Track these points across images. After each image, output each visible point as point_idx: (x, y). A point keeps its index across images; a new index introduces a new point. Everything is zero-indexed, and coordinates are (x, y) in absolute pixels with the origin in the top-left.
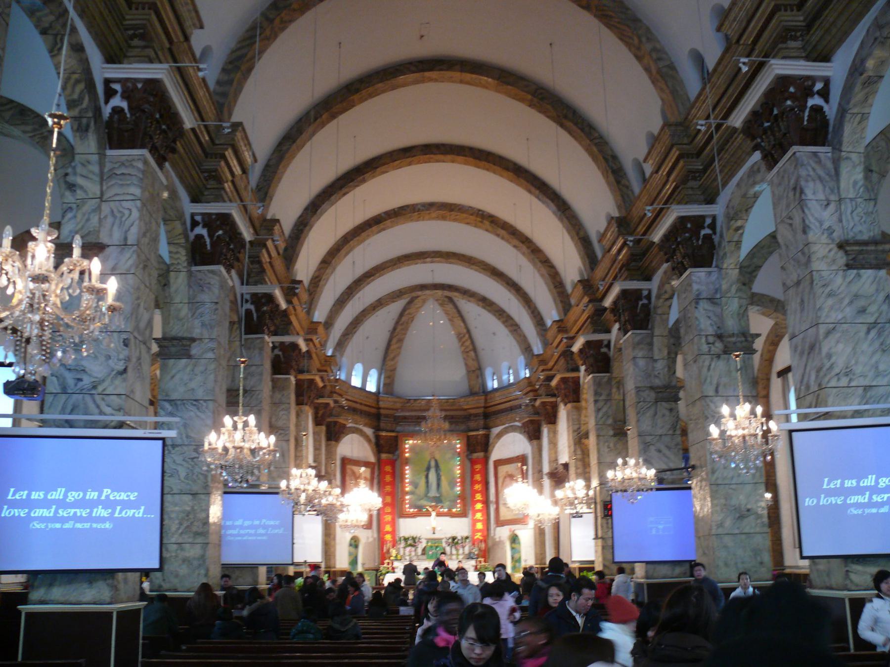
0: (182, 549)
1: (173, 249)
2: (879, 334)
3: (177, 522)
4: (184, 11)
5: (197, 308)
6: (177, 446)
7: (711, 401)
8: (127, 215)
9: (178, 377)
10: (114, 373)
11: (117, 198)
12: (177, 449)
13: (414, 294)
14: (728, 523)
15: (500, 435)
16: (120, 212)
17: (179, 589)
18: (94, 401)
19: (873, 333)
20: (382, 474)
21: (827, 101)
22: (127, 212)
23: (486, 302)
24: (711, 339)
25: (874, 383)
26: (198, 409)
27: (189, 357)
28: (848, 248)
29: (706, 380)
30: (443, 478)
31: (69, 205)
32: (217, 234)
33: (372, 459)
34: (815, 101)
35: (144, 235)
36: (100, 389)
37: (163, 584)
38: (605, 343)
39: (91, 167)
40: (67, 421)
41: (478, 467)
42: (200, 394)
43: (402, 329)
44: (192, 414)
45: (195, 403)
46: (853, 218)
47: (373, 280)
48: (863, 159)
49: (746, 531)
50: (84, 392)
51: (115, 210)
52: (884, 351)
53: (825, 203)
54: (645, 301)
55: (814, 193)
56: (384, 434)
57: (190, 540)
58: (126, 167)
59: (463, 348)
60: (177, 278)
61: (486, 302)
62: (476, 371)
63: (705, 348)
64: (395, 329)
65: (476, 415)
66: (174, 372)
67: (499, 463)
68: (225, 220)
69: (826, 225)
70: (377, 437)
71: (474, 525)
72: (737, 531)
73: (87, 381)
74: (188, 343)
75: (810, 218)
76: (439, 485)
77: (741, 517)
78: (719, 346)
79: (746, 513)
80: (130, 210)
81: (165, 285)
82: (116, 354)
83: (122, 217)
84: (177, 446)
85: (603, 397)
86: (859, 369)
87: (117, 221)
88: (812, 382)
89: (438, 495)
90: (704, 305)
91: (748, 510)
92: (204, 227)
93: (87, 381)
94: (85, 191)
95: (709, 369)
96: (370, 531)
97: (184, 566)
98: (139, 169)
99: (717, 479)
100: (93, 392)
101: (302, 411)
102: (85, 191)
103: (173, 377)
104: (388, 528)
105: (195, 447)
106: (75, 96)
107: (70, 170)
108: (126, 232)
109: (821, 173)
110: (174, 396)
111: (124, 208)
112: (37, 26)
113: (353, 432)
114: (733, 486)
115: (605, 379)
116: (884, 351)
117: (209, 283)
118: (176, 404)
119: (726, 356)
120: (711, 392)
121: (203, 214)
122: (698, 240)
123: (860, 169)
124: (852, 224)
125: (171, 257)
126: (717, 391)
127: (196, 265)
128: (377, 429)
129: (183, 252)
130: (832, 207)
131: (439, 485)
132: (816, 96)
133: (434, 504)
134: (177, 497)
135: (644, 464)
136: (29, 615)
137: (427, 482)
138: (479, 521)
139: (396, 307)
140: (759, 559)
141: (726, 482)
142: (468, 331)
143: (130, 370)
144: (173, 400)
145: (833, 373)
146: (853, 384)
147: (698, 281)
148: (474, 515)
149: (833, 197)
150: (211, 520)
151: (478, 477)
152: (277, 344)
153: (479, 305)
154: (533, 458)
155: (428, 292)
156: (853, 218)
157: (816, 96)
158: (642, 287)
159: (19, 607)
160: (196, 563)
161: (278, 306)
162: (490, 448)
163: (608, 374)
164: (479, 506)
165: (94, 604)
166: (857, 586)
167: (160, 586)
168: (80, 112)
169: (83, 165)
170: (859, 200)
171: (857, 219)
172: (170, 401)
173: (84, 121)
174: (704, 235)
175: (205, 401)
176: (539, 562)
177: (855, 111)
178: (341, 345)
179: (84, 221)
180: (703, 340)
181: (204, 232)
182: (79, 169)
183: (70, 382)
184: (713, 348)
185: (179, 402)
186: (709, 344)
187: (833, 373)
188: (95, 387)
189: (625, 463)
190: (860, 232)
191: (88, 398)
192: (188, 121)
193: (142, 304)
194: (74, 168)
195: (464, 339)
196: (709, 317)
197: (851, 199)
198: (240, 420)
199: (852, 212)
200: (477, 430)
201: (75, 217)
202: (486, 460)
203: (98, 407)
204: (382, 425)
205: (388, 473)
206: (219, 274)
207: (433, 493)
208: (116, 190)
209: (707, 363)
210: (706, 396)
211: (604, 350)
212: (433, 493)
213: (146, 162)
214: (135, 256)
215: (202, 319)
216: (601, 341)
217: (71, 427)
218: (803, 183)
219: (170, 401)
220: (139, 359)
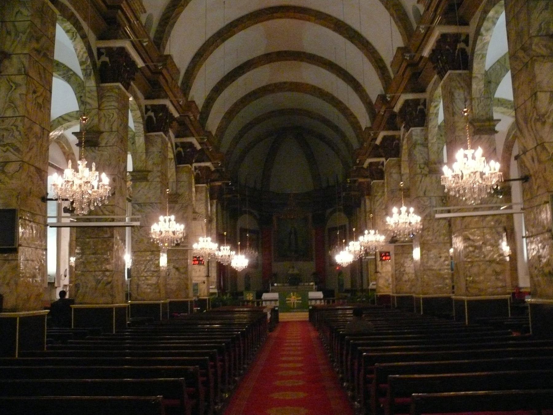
1: (136, 125)
3: (143, 266)
4: (136, 6)
7: (422, 199)
8: (112, 117)
15: (331, 213)
16: (108, 115)
21: (467, 45)
22: (112, 115)
24: (422, 166)
26: (152, 208)
27: (148, 181)
28: (475, 124)
29: (419, 188)
34: (461, 45)
35: (121, 125)
39: (93, 93)
40: (87, 219)
42: (153, 200)
44: (149, 210)
45: (150, 204)
48: (484, 77)
51: (106, 114)
54: (397, 141)
60: (139, 139)
63: (419, 171)
68: (164, 108)
75: (456, 108)
78: (427, 169)
80: (113, 114)
81: (133, 143)
90: (419, 148)
92: (152, 111)
95: (421, 182)
98: (116, 93)
106: (84, 60)
108: (112, 125)
110: (140, 201)
112: (64, 29)
115: (381, 184)
118: (141, 206)
120: (421, 194)
121: (106, 48)
122: (416, 112)
124: (478, 111)
125: (135, 129)
126: (425, 194)
129: (142, 126)
130: (468, 103)
132: (462, 43)
134: (143, 253)
135: (378, 234)
136: (75, 309)
143: (116, 193)
144: (140, 203)
147: (416, 134)
149: (468, 97)
150: (161, 265)
152: (197, 167)
157: (462, 43)
159: (71, 306)
161: (195, 148)
165: (104, 304)
168: (86, 66)
169: (89, 92)
171: (480, 108)
173: (88, 71)
174: (420, 109)
175: (156, 203)
177: (479, 52)
180: (418, 166)
181: (152, 114)
182: (87, 94)
185: (142, 205)
189: (369, 233)
192: (140, 64)
193: (121, 160)
196: (422, 154)
197: (478, 98)
198: (167, 218)
203: (102, 211)
206: (162, 137)
209: (420, 179)
210: (419, 197)
213: (119, 89)
214: (117, 137)
216: (379, 162)
217: (90, 221)
218: (453, 90)
220: (121, 187)
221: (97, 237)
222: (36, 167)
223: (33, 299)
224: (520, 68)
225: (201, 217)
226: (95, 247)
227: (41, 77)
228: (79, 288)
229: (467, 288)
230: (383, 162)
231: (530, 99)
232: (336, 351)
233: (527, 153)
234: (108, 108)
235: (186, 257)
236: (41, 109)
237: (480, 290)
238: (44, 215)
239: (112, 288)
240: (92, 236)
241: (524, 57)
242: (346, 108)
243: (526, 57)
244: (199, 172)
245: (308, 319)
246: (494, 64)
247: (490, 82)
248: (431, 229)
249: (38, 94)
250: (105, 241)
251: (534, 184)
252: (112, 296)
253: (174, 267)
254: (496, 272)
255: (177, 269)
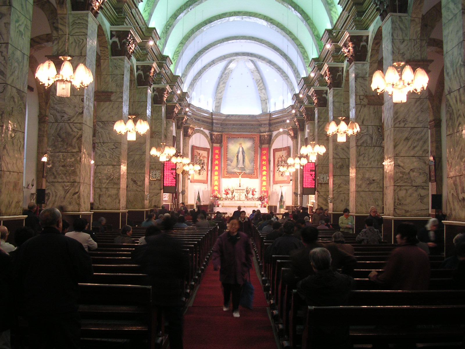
0: (108, 191)
1: (101, 49)
2: (421, 104)
5: (114, 77)
6: (106, 143)
9: (105, 110)
10: (78, 113)
11: (77, 34)
12: (105, 144)
13: (232, 58)
14: (364, 185)
15: (277, 136)
16: (79, 40)
17: (107, 209)
18: (70, 126)
19: (418, 103)
20: (213, 154)
22: (81, 41)
23: (270, 63)
25: (416, 126)
27: (111, 101)
30: (246, 157)
31: (56, 37)
32: (123, 41)
33: (208, 147)
36: (72, 120)
37: (99, 206)
38: (325, 91)
41: (265, 152)
43: (226, 77)
46: (414, 49)
47: (209, 51)
48: (421, 21)
49: (372, 190)
50: (65, 122)
52: (422, 111)
53: (402, 41)
55: (397, 36)
56: (216, 133)
57: (112, 186)
58: (80, 19)
59: (259, 88)
61: (270, 63)
62: (264, 101)
64: (222, 77)
65: (265, 124)
66: (103, 108)
67: (275, 150)
69: (401, 52)
70: (211, 135)
71: (262, 183)
72: (367, 190)
73: (66, 117)
74: (110, 94)
76: (243, 161)
77: (370, 183)
79: (373, 181)
80: (83, 40)
82: (78, 105)
83: (79, 43)
84: (106, 143)
85: (322, 120)
86: (409, 119)
87: (77, 45)
88: (390, 124)
89: (243, 167)
91: (374, 180)
93: (66, 117)
94: (63, 31)
96: (206, 185)
97: (109, 199)
99: (360, 165)
100: (69, 122)
101: (169, 122)
102: (63, 31)
103: (103, 110)
104: (216, 183)
105: (114, 143)
107: (55, 21)
108: (81, 50)
109: (402, 26)
111: (81, 39)
113: (198, 132)
114: (367, 169)
115: (324, 111)
116: (422, 111)
117: (120, 65)
118: (105, 123)
119: (369, 106)
121: (116, 31)
122: (359, 48)
123: (419, 25)
124: (413, 52)
127: (113, 56)
128: (212, 130)
131: (243, 161)
133: (240, 171)
137: (238, 159)
138: (264, 181)
139: (218, 68)
140: (377, 203)
141: (364, 167)
142: (262, 78)
145: (398, 121)
146: (406, 126)
148: (262, 178)
151: (264, 158)
153: (267, 65)
154: (293, 149)
155: (239, 57)
156: (414, 49)
158: (362, 35)
160: (114, 197)
162: (271, 143)
163: (326, 108)
164: (264, 173)
165: (72, 212)
166: (398, 214)
167: (98, 207)
170: (418, 40)
171: (416, 49)
172: (102, 122)
176: (294, 203)
178: (192, 85)
179: (62, 45)
182: (60, 21)
183: (59, 118)
184: (362, 102)
185: (106, 122)
186: (360, 99)
187: (398, 121)
188: (69, 120)
190: (417, 55)
191: (67, 124)
194: (57, 20)
195: (259, 83)
196: (362, 86)
197: (414, 40)
199: (414, 46)
200: (265, 132)
201: (58, 43)
202: (269, 149)
204: (214, 128)
205: (217, 154)
207: (241, 165)
208: (76, 30)
211: (324, 95)
212: (241, 165)
215: (117, 82)
216: (323, 90)
219: (102, 122)
221: (66, 151)
222: (17, 89)
223: (13, 205)
224: (450, 18)
225: (157, 135)
226: (64, 160)
227: (23, 8)
228: (49, 196)
229: (394, 208)
230: (327, 91)
231: (457, 47)
232: (218, 128)
233: (452, 94)
234: (79, 34)
235: (143, 172)
236: (22, 36)
237: (407, 211)
238: (23, 131)
239: (79, 197)
240: (62, 151)
241: (454, 9)
242: (291, 60)
243: (456, 9)
244: (157, 94)
245: (303, 206)
246: (430, 10)
247: (426, 26)
248: (366, 155)
249: (20, 23)
250: (73, 156)
251: (456, 121)
252: (79, 205)
253: (132, 180)
254: (421, 196)
255: (135, 182)
